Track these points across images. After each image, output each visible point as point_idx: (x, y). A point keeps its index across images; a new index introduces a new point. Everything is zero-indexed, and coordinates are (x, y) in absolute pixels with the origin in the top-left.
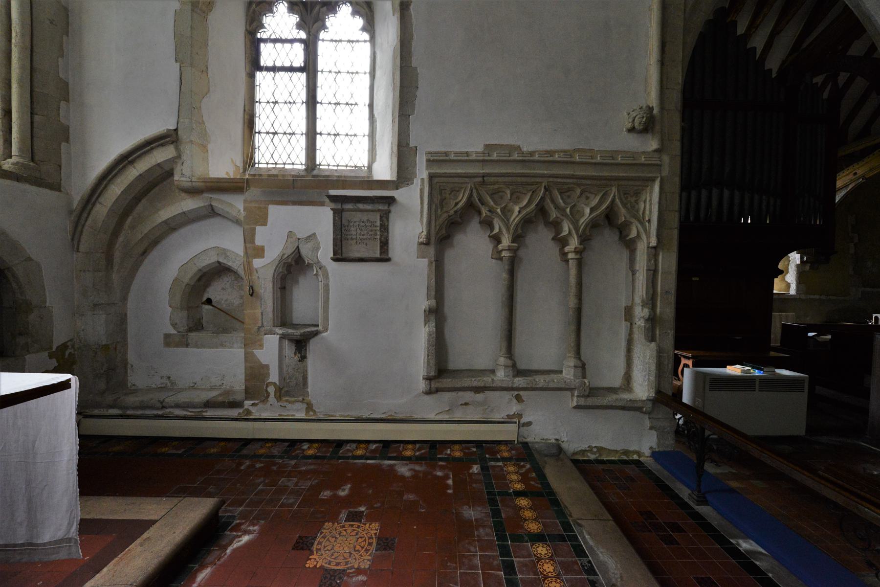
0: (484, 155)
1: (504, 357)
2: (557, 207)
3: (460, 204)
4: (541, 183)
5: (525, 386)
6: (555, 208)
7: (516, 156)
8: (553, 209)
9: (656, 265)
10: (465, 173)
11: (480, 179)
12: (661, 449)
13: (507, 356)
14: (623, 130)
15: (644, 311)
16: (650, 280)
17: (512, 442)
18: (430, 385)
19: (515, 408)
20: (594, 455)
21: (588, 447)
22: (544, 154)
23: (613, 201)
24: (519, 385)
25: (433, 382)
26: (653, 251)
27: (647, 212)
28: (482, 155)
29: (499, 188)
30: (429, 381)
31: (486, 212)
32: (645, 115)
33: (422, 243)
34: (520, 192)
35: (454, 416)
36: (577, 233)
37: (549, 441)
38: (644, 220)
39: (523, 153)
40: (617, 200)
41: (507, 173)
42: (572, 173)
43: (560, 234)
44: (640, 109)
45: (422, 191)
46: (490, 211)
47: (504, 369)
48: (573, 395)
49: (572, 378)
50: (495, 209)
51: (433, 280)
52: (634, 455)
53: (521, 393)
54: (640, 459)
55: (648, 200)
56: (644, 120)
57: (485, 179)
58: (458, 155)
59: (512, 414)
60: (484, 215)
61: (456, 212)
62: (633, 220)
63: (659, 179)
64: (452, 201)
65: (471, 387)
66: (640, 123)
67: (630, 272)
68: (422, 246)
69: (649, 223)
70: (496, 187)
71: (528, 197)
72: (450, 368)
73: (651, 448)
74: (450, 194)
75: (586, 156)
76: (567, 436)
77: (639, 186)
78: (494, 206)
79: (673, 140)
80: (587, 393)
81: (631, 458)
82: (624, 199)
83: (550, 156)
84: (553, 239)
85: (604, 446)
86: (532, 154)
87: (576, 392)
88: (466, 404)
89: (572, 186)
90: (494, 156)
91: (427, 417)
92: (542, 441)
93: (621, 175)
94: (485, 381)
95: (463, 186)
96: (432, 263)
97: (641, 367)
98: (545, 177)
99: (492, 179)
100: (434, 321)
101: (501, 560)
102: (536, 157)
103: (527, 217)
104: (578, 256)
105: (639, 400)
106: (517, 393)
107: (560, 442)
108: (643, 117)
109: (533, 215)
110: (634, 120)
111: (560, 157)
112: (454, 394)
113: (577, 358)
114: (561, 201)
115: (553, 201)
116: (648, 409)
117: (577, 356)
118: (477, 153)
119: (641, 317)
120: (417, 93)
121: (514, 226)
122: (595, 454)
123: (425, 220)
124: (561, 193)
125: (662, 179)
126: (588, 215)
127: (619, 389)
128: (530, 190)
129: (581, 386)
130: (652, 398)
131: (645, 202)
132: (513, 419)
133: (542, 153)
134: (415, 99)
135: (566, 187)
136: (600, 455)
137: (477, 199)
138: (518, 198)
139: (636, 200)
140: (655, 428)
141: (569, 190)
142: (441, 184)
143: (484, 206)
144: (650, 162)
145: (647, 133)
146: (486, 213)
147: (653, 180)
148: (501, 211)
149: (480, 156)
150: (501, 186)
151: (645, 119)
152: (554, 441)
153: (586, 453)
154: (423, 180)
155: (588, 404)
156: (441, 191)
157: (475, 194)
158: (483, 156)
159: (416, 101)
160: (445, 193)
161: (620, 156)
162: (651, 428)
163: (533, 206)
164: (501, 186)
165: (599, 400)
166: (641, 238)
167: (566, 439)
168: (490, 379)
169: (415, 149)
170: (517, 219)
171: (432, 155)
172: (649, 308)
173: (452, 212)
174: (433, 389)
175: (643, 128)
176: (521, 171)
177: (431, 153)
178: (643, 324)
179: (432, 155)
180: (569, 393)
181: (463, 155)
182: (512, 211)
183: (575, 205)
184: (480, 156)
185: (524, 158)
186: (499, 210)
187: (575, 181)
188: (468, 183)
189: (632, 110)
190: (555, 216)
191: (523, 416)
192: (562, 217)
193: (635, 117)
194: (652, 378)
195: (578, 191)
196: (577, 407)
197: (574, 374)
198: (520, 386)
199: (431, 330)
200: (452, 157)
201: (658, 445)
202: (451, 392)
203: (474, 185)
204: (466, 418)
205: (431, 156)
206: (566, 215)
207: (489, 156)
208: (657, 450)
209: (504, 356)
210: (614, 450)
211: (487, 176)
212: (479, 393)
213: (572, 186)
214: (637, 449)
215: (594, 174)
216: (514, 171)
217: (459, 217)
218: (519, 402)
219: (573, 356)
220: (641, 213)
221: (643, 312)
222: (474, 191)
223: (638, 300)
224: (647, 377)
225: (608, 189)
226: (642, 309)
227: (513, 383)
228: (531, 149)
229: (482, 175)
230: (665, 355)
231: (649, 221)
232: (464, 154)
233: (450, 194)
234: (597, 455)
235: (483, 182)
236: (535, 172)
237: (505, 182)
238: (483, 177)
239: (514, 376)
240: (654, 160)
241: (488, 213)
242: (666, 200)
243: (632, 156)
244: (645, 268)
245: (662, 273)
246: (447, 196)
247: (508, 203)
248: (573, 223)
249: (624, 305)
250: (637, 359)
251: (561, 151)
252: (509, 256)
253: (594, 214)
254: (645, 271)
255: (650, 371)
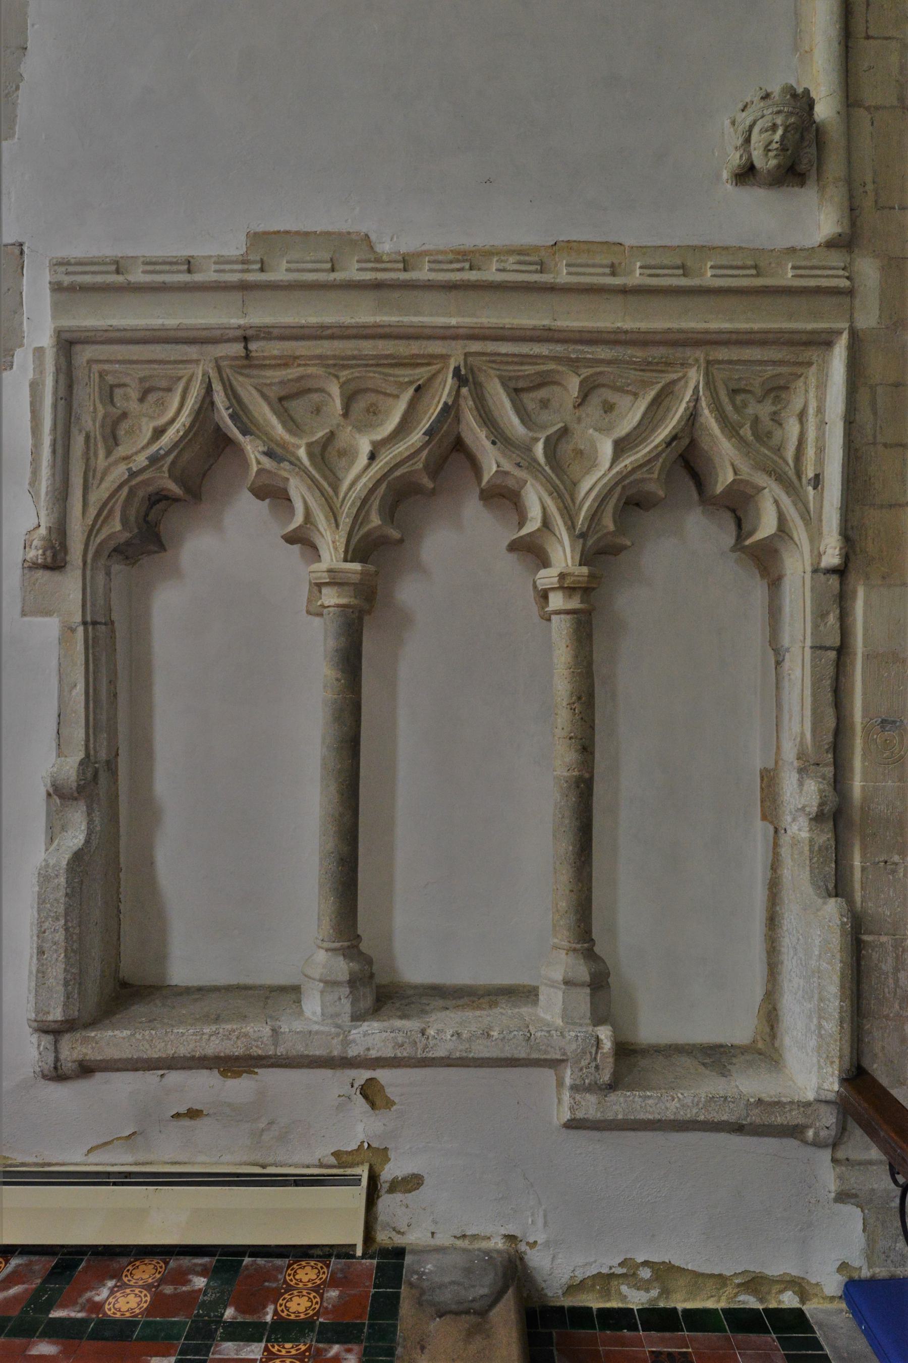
0: (246, 267)
1: (327, 950)
2: (499, 437)
3: (171, 435)
4: (444, 358)
5: (388, 1052)
6: (494, 443)
7: (352, 271)
8: (487, 444)
9: (845, 631)
10: (178, 329)
11: (237, 349)
12: (881, 1272)
13: (337, 945)
14: (718, 177)
15: (805, 788)
16: (827, 683)
17: (344, 1252)
18: (56, 1051)
19: (360, 1128)
20: (642, 1293)
21: (621, 1265)
22: (451, 262)
23: (692, 417)
24: (368, 1049)
25: (66, 1041)
26: (834, 581)
27: (810, 452)
28: (240, 267)
29: (300, 379)
30: (50, 1038)
31: (257, 453)
32: (779, 120)
33: (34, 566)
34: (377, 392)
35: (151, 1157)
36: (571, 527)
37: (484, 1245)
38: (799, 477)
39: (379, 260)
40: (706, 412)
41: (323, 327)
42: (546, 322)
43: (750, 534)
44: (763, 98)
45: (35, 387)
46: (269, 454)
47: (322, 992)
48: (560, 1084)
49: (559, 1022)
50: (291, 449)
51: (80, 687)
52: (781, 1292)
53: (382, 1075)
54: (804, 1308)
55: (811, 411)
56: (777, 136)
57: (253, 346)
58: (158, 268)
59: (353, 1146)
60: (255, 468)
61: (154, 460)
62: (761, 479)
63: (845, 336)
64: (144, 420)
65: (200, 1058)
66: (767, 149)
67: (772, 652)
68: (40, 573)
69: (815, 488)
70: (292, 373)
71: (401, 406)
72: (173, 983)
73: (844, 1267)
74: (142, 400)
75: (285, 362)
76: (545, 1224)
77: (781, 363)
78: (287, 437)
79: (894, 208)
80: (606, 1076)
81: (773, 1305)
82: (729, 408)
83: (471, 269)
84: (734, 549)
85: (677, 1263)
86: (406, 262)
87: (569, 1072)
88: (193, 1114)
89: (552, 366)
90: (280, 274)
91: (60, 1159)
92: (459, 1243)
93: (714, 325)
94: (246, 1035)
95: (181, 373)
96: (73, 630)
97: (802, 982)
98: (455, 337)
99: (275, 348)
100: (84, 827)
101: (785, 1354)
102: (423, 274)
103: (398, 473)
104: (575, 603)
105: (792, 1103)
106: (366, 1074)
107: (523, 1247)
108: (774, 128)
109: (420, 465)
110: (748, 141)
111: (503, 270)
112: (152, 1077)
113: (575, 950)
114: (515, 420)
115: (488, 420)
116: (824, 1133)
117: (578, 946)
118: (221, 260)
119: (798, 810)
120: (22, 66)
121: (353, 503)
122: (647, 1290)
123: (44, 484)
124: (516, 393)
125: (854, 335)
126: (607, 465)
127: (743, 1050)
128: (411, 383)
129: (584, 1052)
130: (831, 1096)
131: (802, 416)
132: (352, 1166)
133: (440, 257)
134: (17, 88)
135: (529, 369)
136: (666, 1292)
137: (225, 414)
138: (373, 411)
139: (775, 413)
140: (855, 1196)
141: (544, 381)
142: (106, 367)
143: (248, 437)
144: (812, 283)
145: (802, 184)
146: (258, 463)
147: (825, 342)
148: (311, 455)
149: (232, 271)
150: (311, 370)
151: (780, 132)
152: (498, 1243)
153: (614, 1283)
154: (39, 352)
155: (610, 1116)
156: (109, 394)
157: (220, 398)
158: (243, 271)
159: (20, 92)
160: (126, 397)
161: (709, 264)
162: (843, 1197)
163: (416, 437)
164: (311, 370)
165: (650, 1102)
166: (792, 538)
167: (541, 1238)
168: (267, 1031)
169: (17, 252)
170: (364, 480)
171: (71, 269)
172: (824, 777)
173: (141, 460)
174: (68, 1066)
175: (779, 166)
176: (379, 319)
177: (68, 263)
178: (805, 835)
179: (71, 269)
180: (548, 1075)
181: (175, 268)
182: (348, 454)
183: (565, 432)
184: (232, 271)
185: (381, 276)
186: (302, 453)
187: (559, 349)
188: (197, 361)
189: (741, 106)
190: (494, 468)
191: (392, 1154)
192: (517, 472)
193: (751, 127)
194: (831, 1027)
195: (573, 384)
196: (574, 1125)
197: (564, 1010)
198: (373, 1054)
199: (52, 862)
200: (138, 276)
201: (870, 1255)
202: (140, 1074)
203: (219, 369)
204: (193, 1164)
205: (67, 273)
206: (532, 465)
207: (262, 270)
208: (865, 1273)
209: (325, 945)
210: (712, 1276)
211: (257, 338)
212: (237, 1074)
213: (552, 366)
214: (795, 1272)
215: (619, 325)
216: (347, 320)
217: (167, 475)
218: (373, 1105)
219: (565, 944)
220: (790, 453)
221: (801, 791)
222: (217, 387)
223: (789, 752)
224: (815, 1021)
225: (674, 376)
226: (801, 784)
227: (346, 1043)
228: (408, 244)
229: (239, 333)
230: (884, 939)
231: (817, 481)
232: (176, 263)
233: (142, 400)
234: (654, 1293)
235: (247, 357)
236: (416, 320)
237: (320, 357)
238: (246, 339)
239: (358, 1017)
240: (827, 276)
241: (267, 463)
242: (875, 413)
243: (750, 263)
244: (808, 643)
245: (867, 657)
246: (133, 406)
247: (338, 425)
248: (556, 492)
249: (758, 765)
250: (792, 952)
251: (511, 252)
252: (338, 606)
253: (628, 461)
254: (808, 651)
255: (821, 1000)
